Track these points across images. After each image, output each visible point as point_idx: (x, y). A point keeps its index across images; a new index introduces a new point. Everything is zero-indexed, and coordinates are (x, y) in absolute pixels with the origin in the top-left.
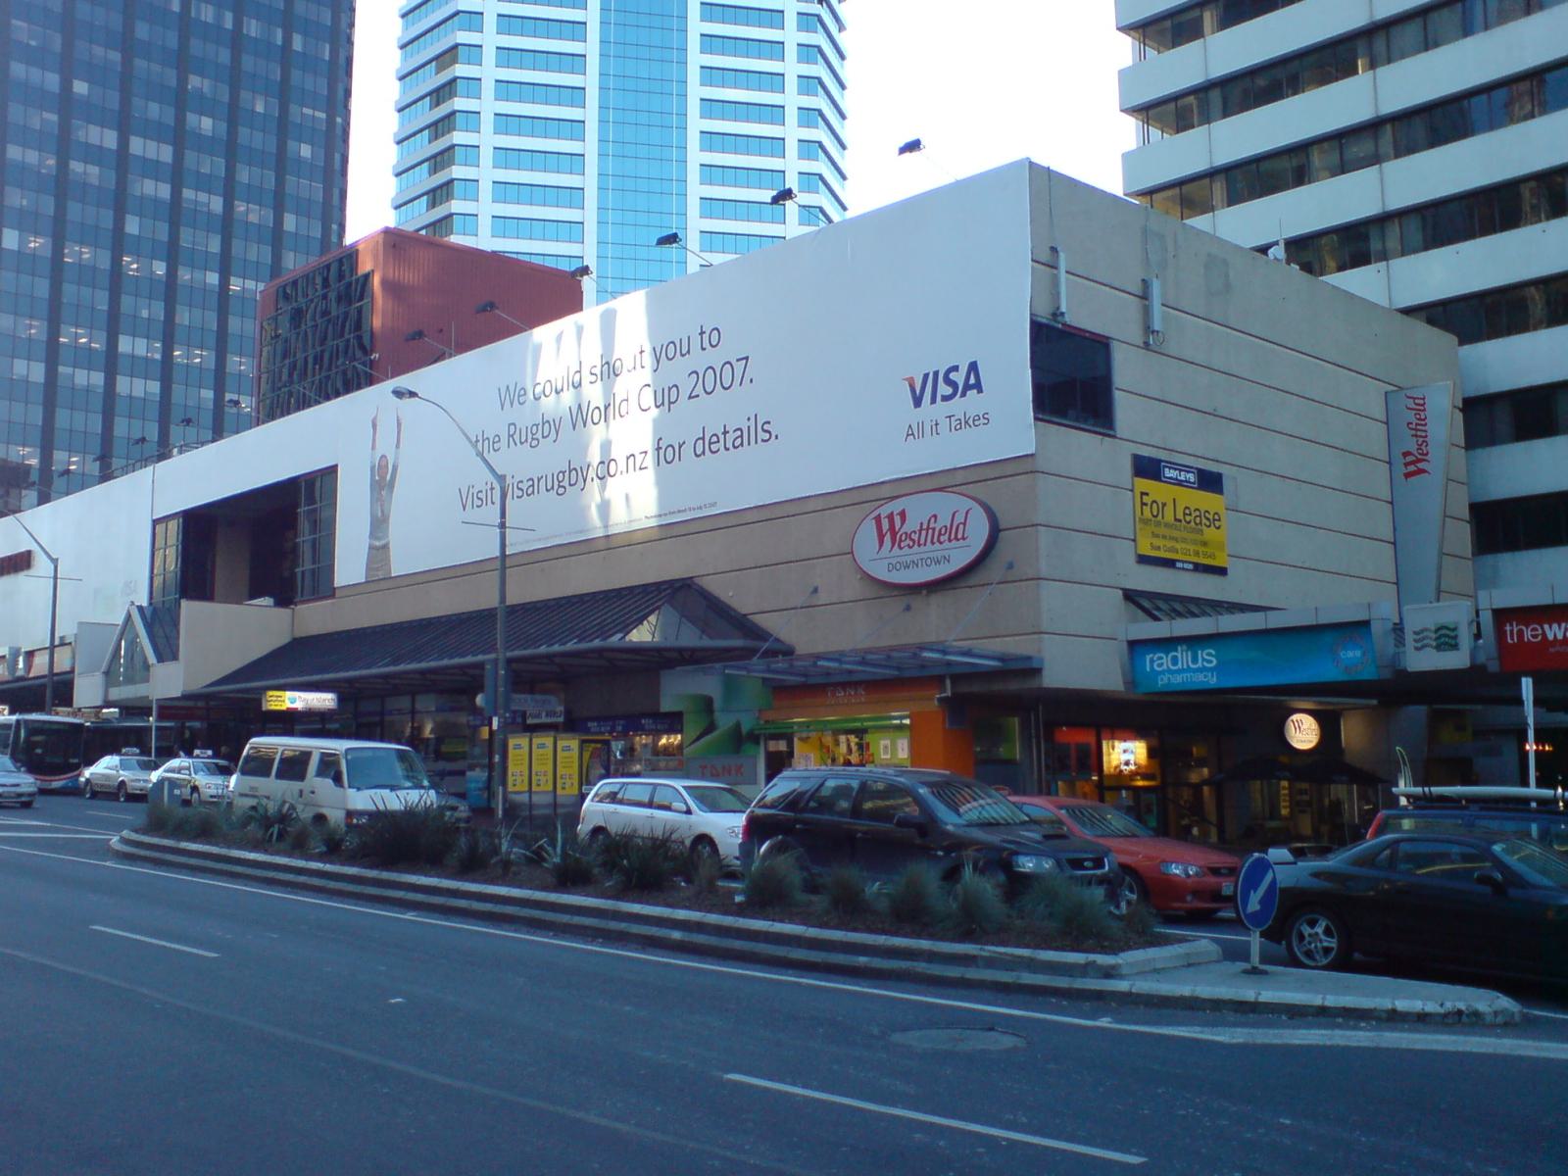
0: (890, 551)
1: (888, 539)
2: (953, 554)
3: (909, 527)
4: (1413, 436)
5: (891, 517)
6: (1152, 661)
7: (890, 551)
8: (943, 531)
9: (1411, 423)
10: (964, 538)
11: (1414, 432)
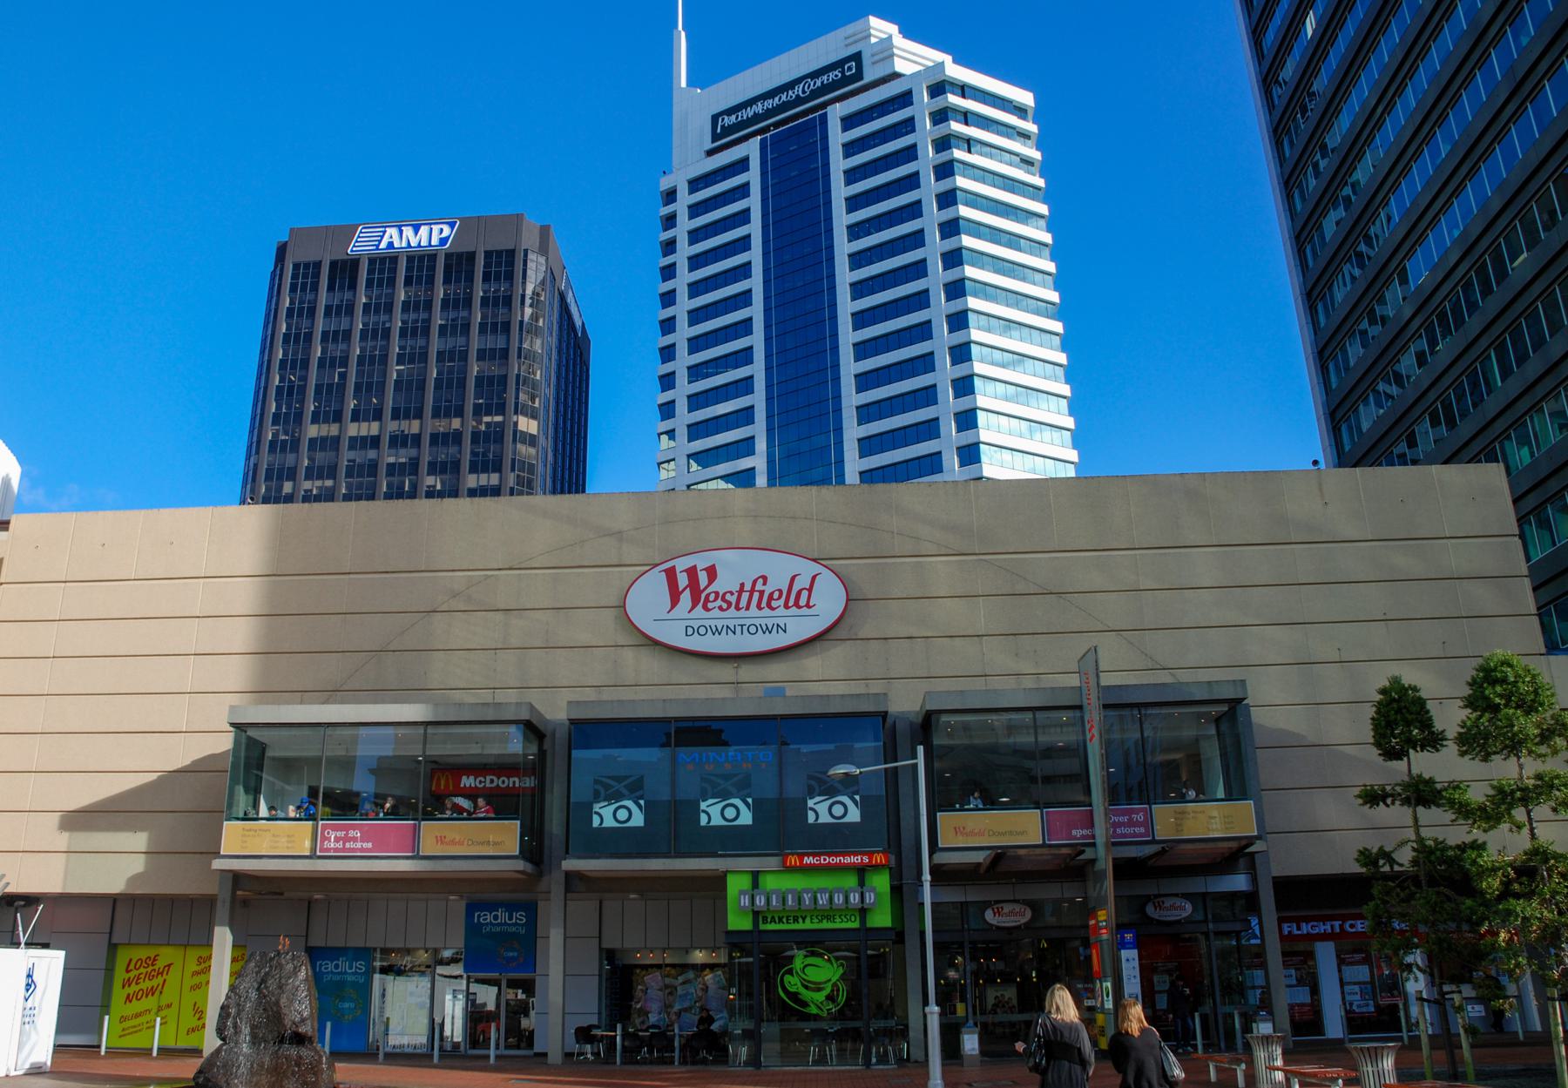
0: (689, 612)
1: (686, 598)
2: (792, 624)
3: (720, 586)
4: (742, 585)
5: (692, 572)
6: (479, 916)
7: (689, 612)
8: (776, 595)
9: (765, 584)
10: (808, 606)
11: (748, 587)
